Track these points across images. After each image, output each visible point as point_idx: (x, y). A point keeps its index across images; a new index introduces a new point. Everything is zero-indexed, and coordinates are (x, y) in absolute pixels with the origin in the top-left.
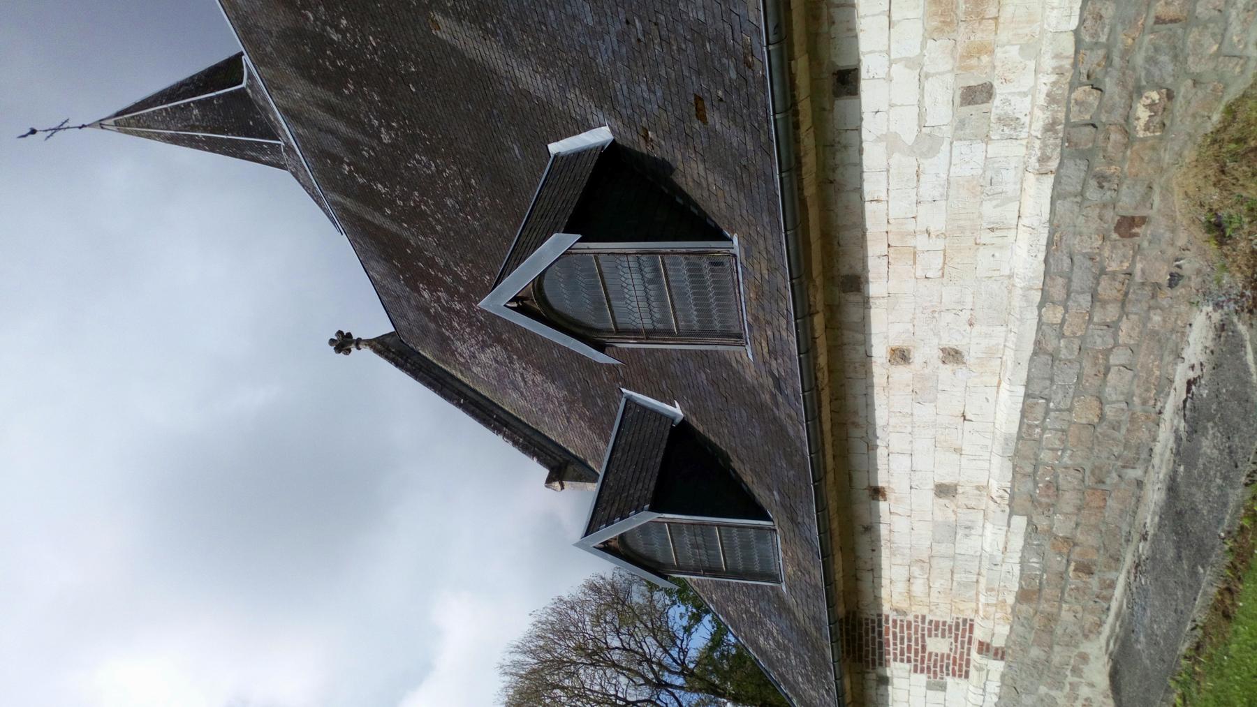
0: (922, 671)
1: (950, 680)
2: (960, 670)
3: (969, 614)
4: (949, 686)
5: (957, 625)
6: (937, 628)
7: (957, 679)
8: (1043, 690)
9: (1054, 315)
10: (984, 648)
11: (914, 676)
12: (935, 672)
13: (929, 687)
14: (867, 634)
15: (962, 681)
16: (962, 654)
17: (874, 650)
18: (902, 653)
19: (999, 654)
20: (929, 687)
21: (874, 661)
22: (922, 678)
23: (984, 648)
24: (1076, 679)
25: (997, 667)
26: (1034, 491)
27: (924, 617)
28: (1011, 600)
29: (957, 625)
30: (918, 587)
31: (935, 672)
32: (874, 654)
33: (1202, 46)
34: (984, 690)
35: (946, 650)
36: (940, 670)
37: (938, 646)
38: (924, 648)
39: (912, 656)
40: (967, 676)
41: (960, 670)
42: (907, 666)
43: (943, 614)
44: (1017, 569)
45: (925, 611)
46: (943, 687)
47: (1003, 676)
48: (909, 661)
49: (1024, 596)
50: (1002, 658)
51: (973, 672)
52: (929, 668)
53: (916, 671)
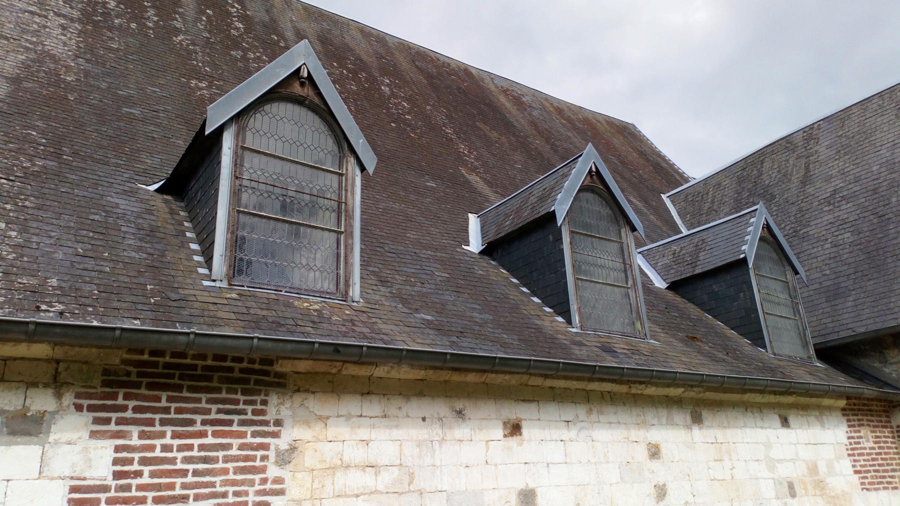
41: (852, 449)
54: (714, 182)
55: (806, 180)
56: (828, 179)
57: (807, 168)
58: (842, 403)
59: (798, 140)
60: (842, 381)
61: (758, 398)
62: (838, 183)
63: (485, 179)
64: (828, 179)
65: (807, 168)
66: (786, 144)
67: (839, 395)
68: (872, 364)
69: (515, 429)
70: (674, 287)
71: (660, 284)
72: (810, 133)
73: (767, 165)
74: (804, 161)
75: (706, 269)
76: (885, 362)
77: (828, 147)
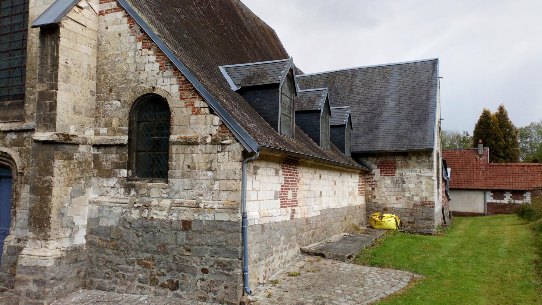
0: (282, 189)
1: (279, 201)
2: (283, 204)
3: (299, 204)
4: (276, 200)
5: (296, 201)
6: (295, 194)
7: (280, 203)
8: (283, 238)
9: (357, 207)
10: (294, 211)
11: (280, 185)
12: (281, 194)
13: (276, 192)
14: (293, 168)
15: (280, 206)
16: (288, 204)
17: (288, 169)
18: (288, 181)
19: (292, 218)
20: (276, 192)
21: (284, 169)
22: (279, 189)
23: (294, 211)
24: (288, 248)
25: (288, 218)
26: (325, 213)
27: (298, 189)
28: (306, 216)
29: (296, 201)
30: (305, 187)
31: (281, 194)
32: (287, 169)
33: (362, 252)
34: (280, 215)
35: (289, 198)
36: (281, 195)
37: (290, 195)
38: (289, 189)
39: (287, 185)
40: (282, 207)
41: (283, 204)
42: (283, 182)
43: (299, 196)
44: (312, 216)
45: (299, 189)
46: (276, 198)
47: (285, 221)
48: (285, 183)
49: (307, 220)
50: (291, 219)
51: (284, 209)
52: (283, 192)
53: (282, 186)
54: (315, 78)
55: (351, 92)
56: (358, 94)
57: (351, 87)
58: (359, 171)
59: (350, 73)
60: (357, 165)
61: (349, 170)
62: (361, 97)
63: (174, 33)
64: (358, 94)
65: (351, 87)
66: (344, 73)
67: (359, 170)
68: (364, 160)
69: (341, 175)
70: (242, 91)
71: (234, 88)
72: (354, 72)
73: (337, 79)
74: (350, 83)
75: (264, 83)
76: (367, 160)
77: (359, 81)
